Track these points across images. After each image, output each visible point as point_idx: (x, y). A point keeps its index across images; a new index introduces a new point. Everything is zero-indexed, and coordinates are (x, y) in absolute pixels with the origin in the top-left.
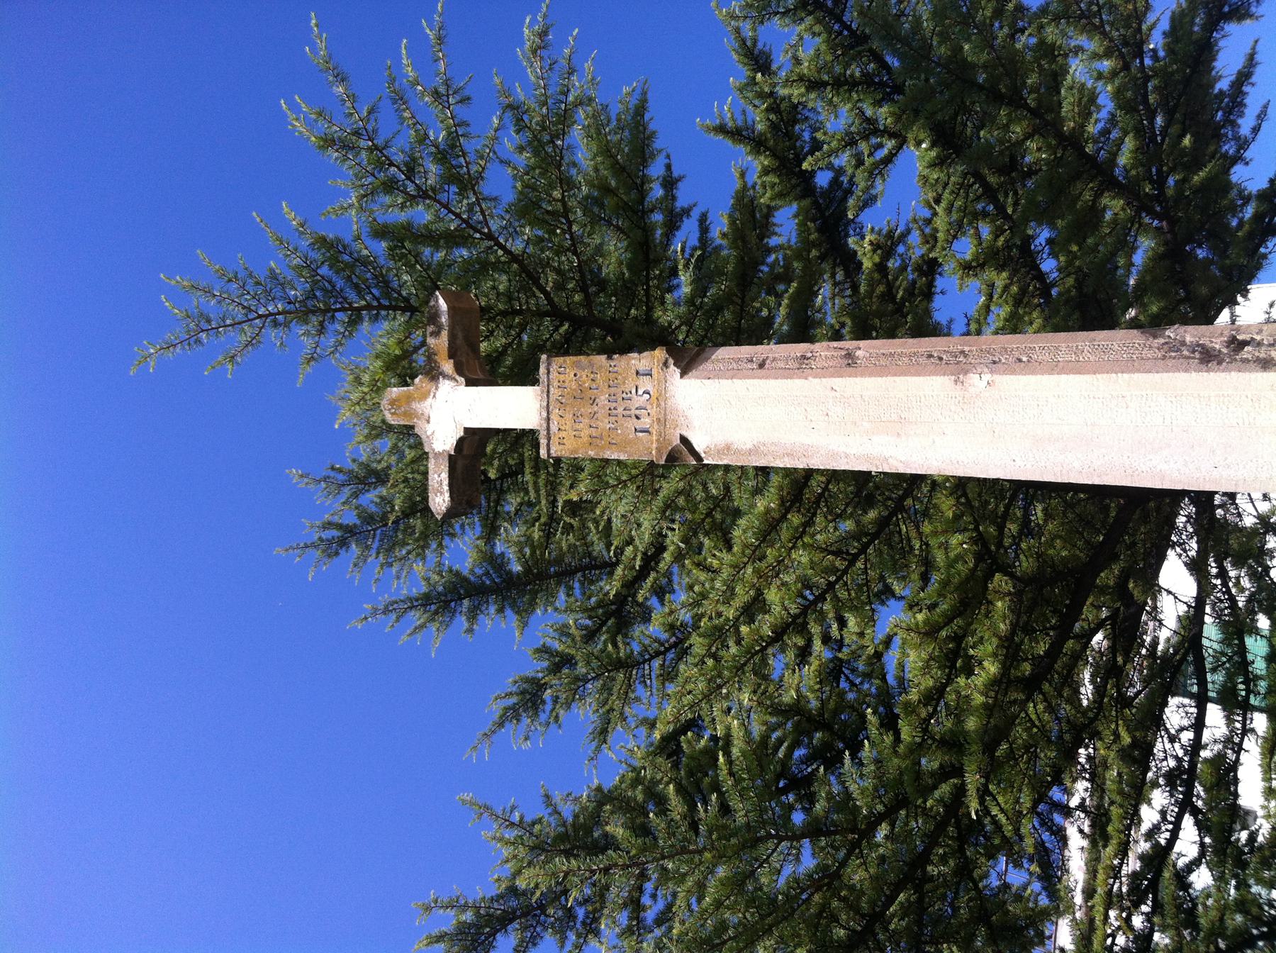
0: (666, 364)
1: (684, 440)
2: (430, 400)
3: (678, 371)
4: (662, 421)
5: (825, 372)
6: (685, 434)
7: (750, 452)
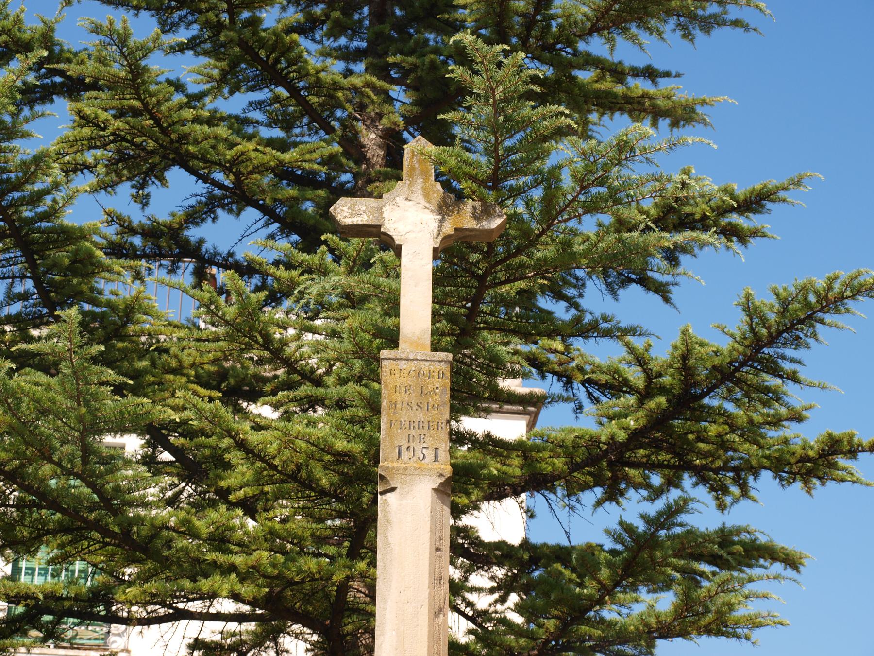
0: (441, 475)
1: (393, 489)
2: (423, 202)
3: (436, 486)
4: (405, 472)
5: (432, 597)
6: (397, 491)
7: (386, 538)
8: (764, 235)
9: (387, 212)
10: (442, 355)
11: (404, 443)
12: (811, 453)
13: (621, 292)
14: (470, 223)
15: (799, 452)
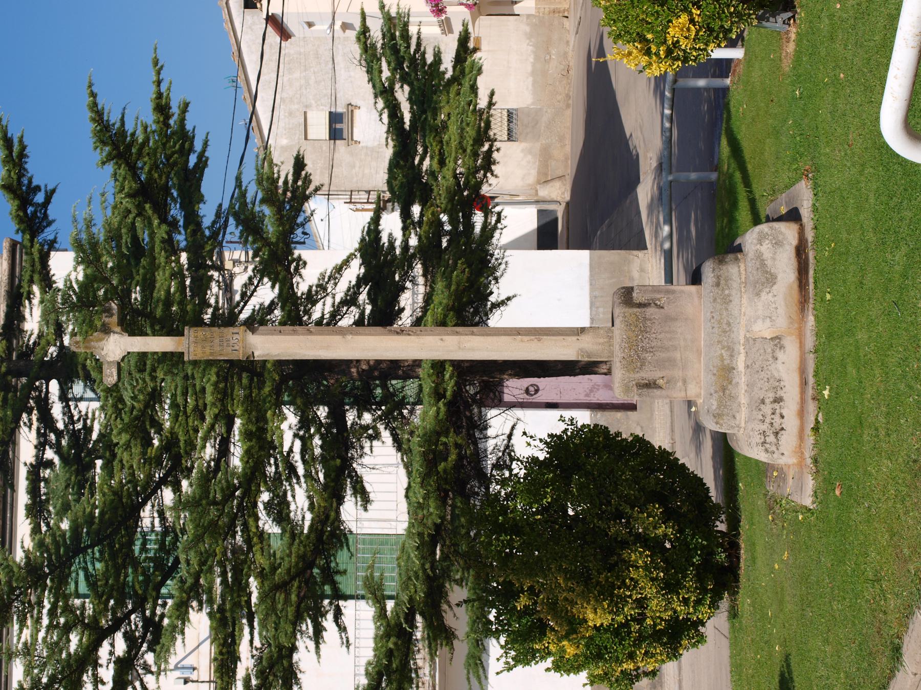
2: (104, 342)
5: (303, 334)
8: (22, 137)
9: (110, 359)
10: (186, 332)
11: (230, 349)
12: (162, 119)
13: (50, 218)
14: (115, 319)
15: (161, 125)
